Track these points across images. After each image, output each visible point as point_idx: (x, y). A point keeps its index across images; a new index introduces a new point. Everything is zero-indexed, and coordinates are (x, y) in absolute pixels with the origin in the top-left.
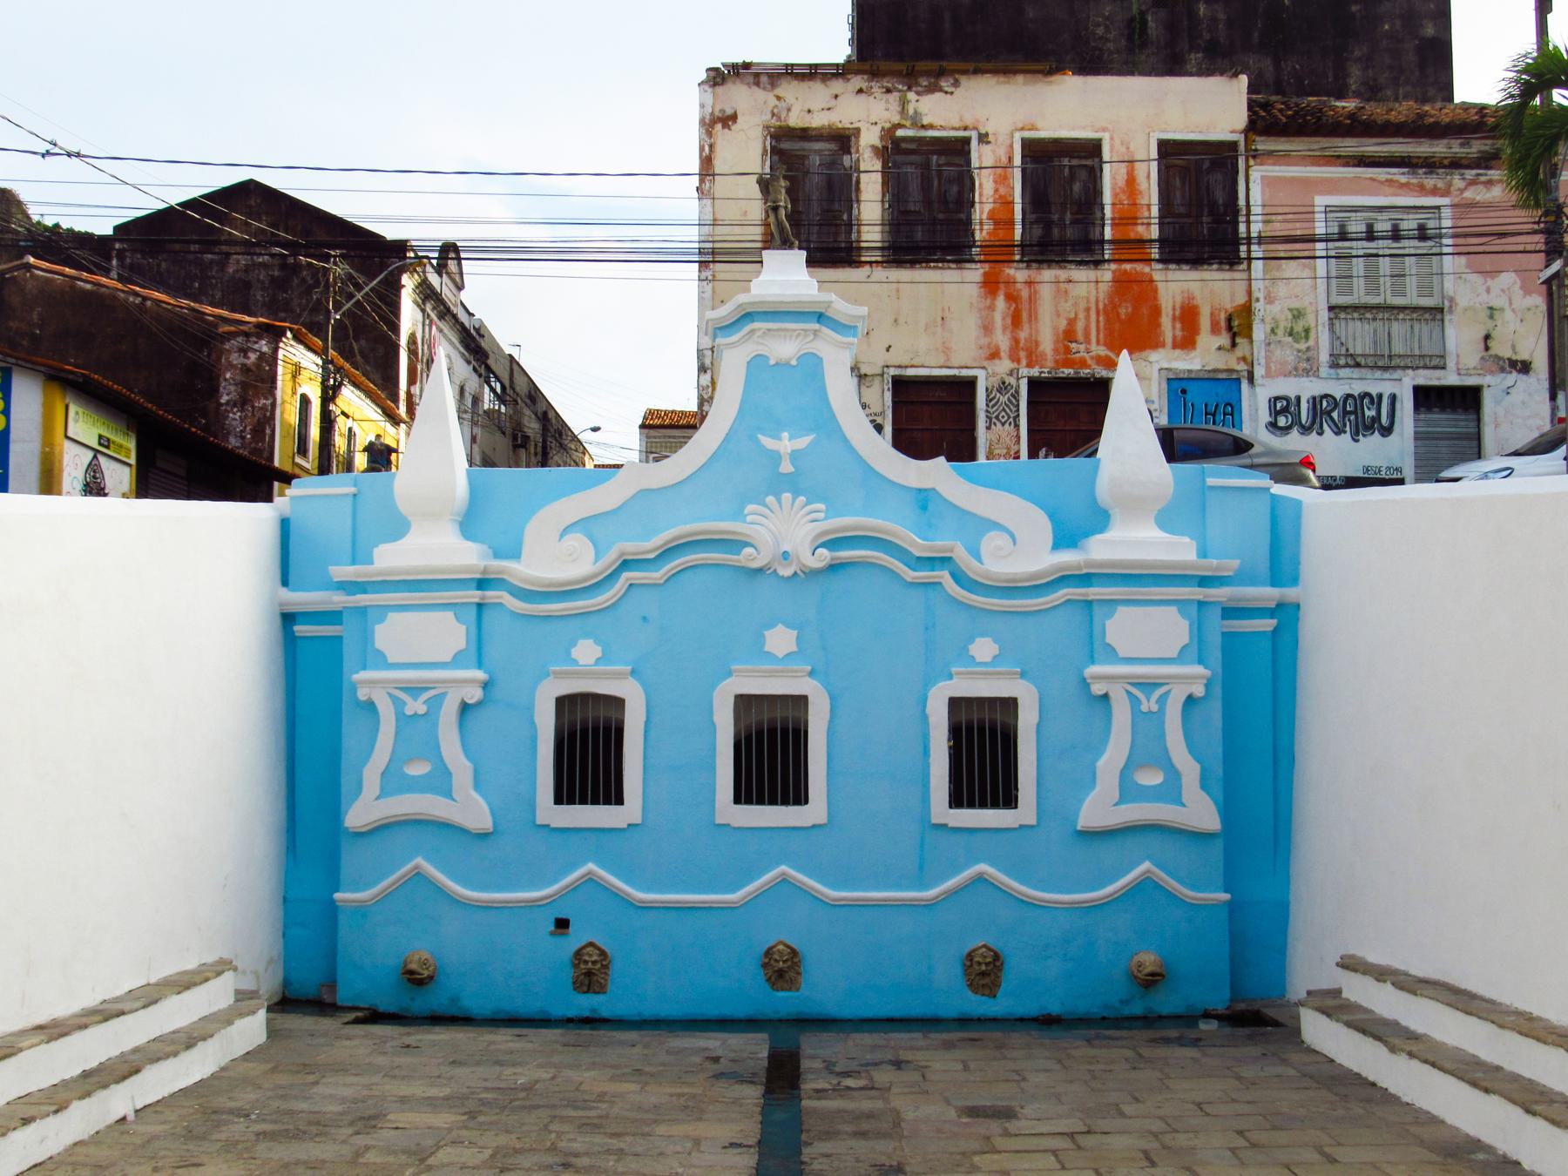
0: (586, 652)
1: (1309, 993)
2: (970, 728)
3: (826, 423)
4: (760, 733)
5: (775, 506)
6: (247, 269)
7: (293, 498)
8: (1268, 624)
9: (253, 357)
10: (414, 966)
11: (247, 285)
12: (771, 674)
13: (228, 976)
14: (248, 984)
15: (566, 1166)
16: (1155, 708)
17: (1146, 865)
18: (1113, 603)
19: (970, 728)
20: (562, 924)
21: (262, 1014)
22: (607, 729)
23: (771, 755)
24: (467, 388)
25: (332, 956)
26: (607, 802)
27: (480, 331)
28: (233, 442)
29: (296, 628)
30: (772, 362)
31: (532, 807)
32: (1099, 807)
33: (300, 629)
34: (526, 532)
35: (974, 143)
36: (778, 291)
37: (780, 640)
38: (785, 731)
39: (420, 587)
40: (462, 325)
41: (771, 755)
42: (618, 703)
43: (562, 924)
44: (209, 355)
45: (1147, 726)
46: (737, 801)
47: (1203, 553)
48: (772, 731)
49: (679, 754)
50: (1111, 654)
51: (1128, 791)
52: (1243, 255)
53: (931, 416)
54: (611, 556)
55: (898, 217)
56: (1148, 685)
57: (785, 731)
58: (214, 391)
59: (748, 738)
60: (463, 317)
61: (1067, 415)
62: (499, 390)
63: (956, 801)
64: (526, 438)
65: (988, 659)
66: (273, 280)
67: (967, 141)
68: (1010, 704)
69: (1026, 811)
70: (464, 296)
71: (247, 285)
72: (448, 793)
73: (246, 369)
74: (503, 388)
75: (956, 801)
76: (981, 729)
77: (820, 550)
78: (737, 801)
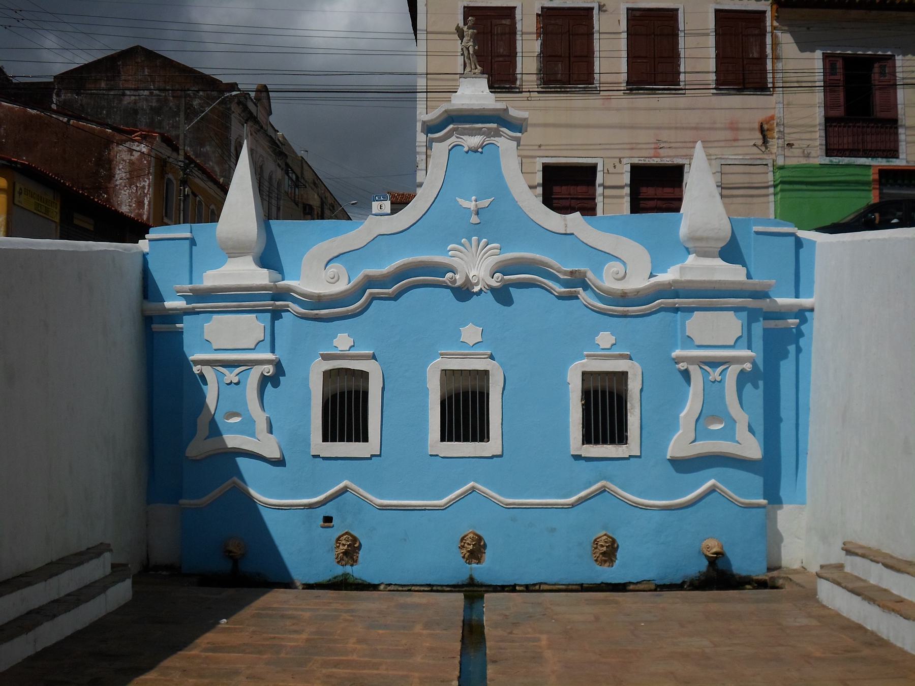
0: (343, 342)
1: (822, 567)
2: (596, 392)
3: (500, 190)
4: (457, 395)
5: (467, 244)
6: (135, 102)
7: (150, 240)
8: (793, 322)
9: (136, 154)
10: (231, 548)
11: (136, 112)
12: (465, 356)
13: (107, 555)
14: (122, 560)
15: (540, 146)
16: (719, 378)
17: (711, 482)
18: (691, 310)
19: (596, 392)
20: (328, 520)
21: (128, 583)
22: (357, 392)
23: (465, 411)
24: (274, 176)
25: (148, 559)
26: (357, 440)
27: (285, 143)
28: (124, 209)
29: (153, 326)
30: (466, 149)
31: (307, 442)
32: (680, 444)
33: (156, 327)
34: (751, 475)
35: (595, 12)
36: (467, 102)
37: (471, 334)
38: (474, 393)
39: (235, 299)
40: (271, 137)
41: (465, 411)
42: (364, 375)
43: (328, 520)
44: (109, 154)
45: (713, 390)
46: (443, 439)
47: (749, 276)
48: (466, 394)
49: (405, 409)
50: (688, 341)
51: (700, 432)
52: (770, 85)
53: (567, 187)
54: (358, 278)
55: (547, 57)
56: (714, 363)
57: (474, 393)
58: (111, 176)
59: (450, 398)
60: (271, 132)
61: (656, 188)
62: (294, 177)
63: (587, 439)
64: (311, 207)
65: (609, 347)
66: (152, 108)
67: (592, 9)
68: (623, 376)
69: (632, 447)
70: (272, 119)
71: (136, 112)
72: (253, 435)
73: (132, 163)
74: (297, 177)
75: (587, 439)
76: (603, 392)
77: (497, 275)
78: (443, 439)
